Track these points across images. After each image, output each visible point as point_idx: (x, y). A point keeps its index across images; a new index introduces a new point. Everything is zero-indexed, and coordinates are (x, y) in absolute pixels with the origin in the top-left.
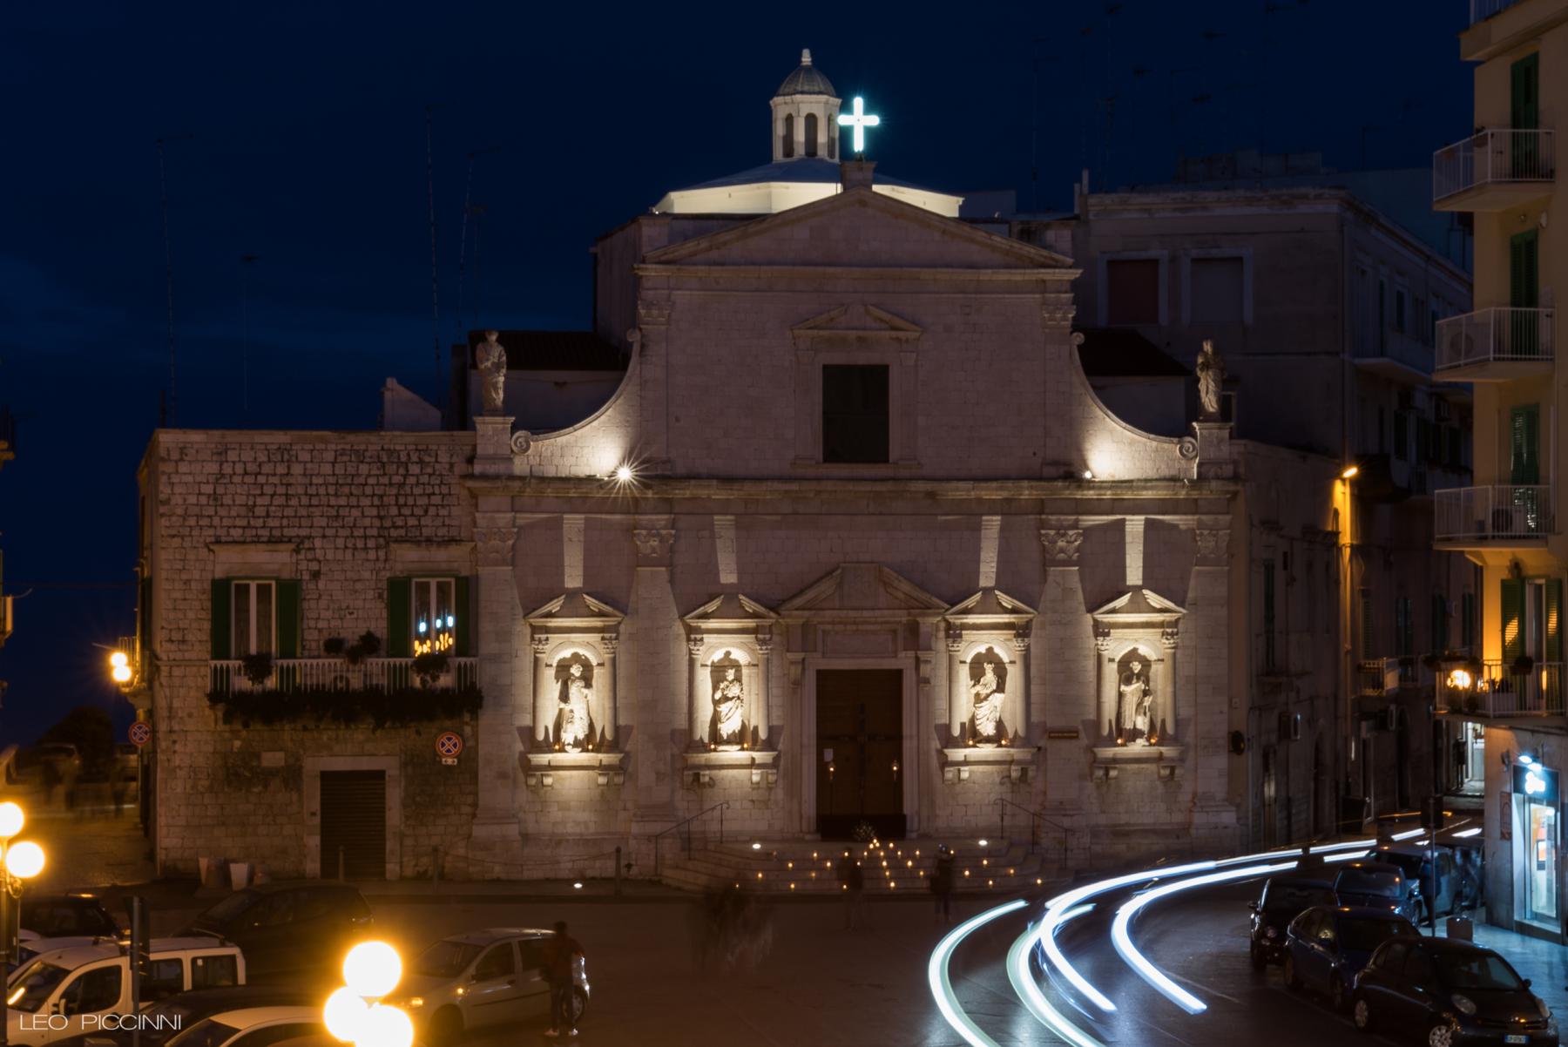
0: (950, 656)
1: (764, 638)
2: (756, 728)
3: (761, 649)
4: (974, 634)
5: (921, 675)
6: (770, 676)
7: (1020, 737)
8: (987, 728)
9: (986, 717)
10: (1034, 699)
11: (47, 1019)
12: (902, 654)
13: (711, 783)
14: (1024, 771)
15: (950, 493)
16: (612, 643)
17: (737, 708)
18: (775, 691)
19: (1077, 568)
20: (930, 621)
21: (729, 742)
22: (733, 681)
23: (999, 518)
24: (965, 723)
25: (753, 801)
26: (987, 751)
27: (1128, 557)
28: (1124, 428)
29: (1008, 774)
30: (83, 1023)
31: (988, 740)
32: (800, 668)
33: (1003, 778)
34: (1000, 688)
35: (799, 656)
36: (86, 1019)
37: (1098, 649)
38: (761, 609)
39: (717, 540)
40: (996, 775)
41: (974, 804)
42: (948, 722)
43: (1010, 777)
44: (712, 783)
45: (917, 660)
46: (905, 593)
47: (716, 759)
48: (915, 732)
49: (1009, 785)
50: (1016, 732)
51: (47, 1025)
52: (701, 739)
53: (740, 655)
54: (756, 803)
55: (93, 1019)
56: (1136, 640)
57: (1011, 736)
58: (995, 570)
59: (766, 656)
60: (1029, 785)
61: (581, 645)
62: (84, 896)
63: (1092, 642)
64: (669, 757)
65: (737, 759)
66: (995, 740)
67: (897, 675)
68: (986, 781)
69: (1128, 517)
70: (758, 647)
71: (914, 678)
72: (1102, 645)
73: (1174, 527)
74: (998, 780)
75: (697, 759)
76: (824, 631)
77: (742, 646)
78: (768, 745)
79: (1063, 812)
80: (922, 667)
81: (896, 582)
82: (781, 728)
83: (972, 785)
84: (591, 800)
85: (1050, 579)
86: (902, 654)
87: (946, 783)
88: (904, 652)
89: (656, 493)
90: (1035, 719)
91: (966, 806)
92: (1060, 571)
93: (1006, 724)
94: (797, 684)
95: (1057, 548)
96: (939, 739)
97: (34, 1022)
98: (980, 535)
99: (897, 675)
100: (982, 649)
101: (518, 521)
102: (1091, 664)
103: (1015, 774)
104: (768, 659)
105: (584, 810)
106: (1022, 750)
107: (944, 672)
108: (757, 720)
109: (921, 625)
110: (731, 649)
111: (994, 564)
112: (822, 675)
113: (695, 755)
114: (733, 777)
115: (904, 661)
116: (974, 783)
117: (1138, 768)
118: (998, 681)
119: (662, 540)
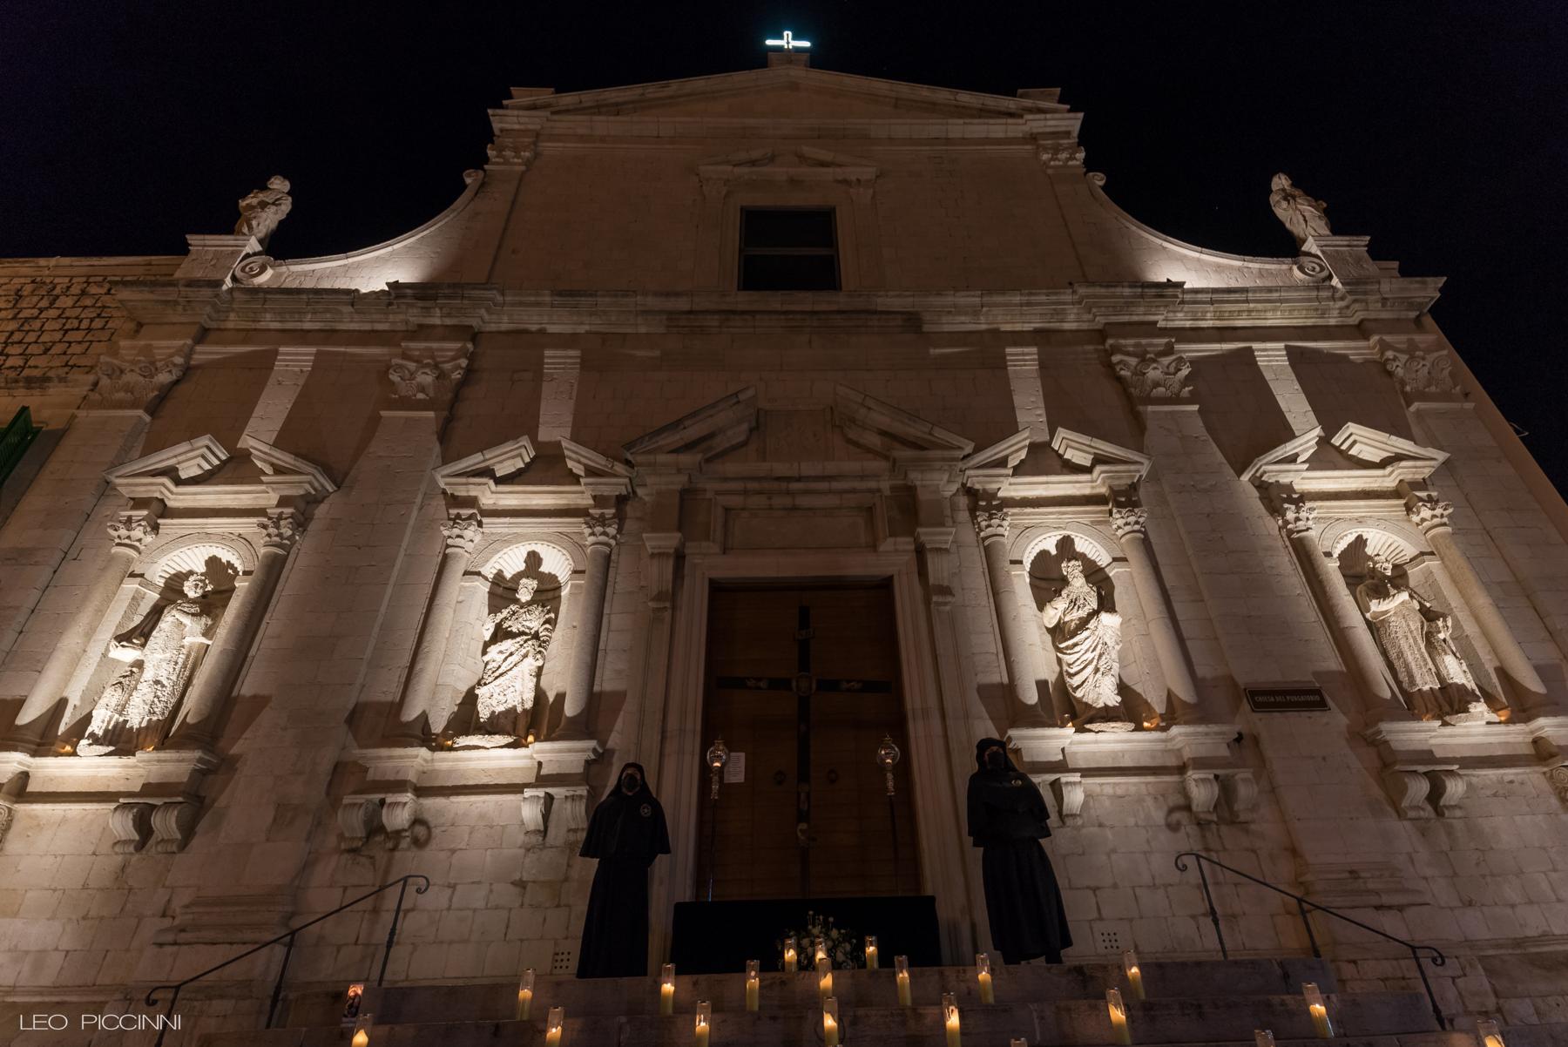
0: (987, 549)
1: (602, 515)
2: (561, 697)
3: (593, 534)
4: (1029, 514)
5: (931, 581)
6: (609, 592)
7: (1184, 703)
8: (1104, 693)
9: (1090, 669)
10: (1187, 630)
11: (47, 1019)
12: (887, 545)
13: (420, 831)
14: (1227, 789)
15: (944, 319)
16: (278, 527)
17: (525, 656)
18: (617, 619)
19: (1196, 407)
20: (942, 484)
21: (494, 726)
22: (529, 603)
23: (1034, 350)
24: (1046, 682)
25: (521, 884)
26: (1112, 740)
27: (1279, 398)
28: (1201, 252)
29: (1181, 801)
30: (83, 1023)
31: (1107, 715)
32: (669, 565)
33: (1171, 811)
34: (1106, 603)
35: (670, 540)
36: (86, 1019)
37: (1290, 532)
38: (599, 461)
39: (545, 385)
40: (1149, 802)
41: (1115, 886)
42: (1006, 680)
43: (1187, 807)
44: (421, 832)
45: (920, 552)
46: (883, 433)
47: (450, 772)
48: (932, 701)
49: (1192, 829)
50: (1170, 695)
51: (46, 1025)
52: (424, 717)
53: (556, 563)
54: (529, 887)
55: (93, 1019)
56: (1360, 521)
57: (1159, 707)
58: (1044, 419)
59: (607, 550)
60: (1244, 826)
61: (223, 539)
62: (890, 784)
63: (1272, 525)
64: (325, 766)
65: (501, 771)
66: (1130, 709)
67: (885, 586)
68: (1131, 821)
69: (1255, 346)
70: (587, 531)
71: (918, 590)
72: (1297, 519)
73: (1342, 359)
74: (1159, 816)
75: (390, 764)
76: (727, 510)
77: (559, 539)
78: (581, 727)
79: (1374, 900)
80: (933, 562)
81: (863, 411)
82: (619, 697)
83: (1095, 830)
84: (85, 887)
85: (1151, 425)
86: (887, 545)
87: (1069, 822)
88: (890, 540)
89: (449, 315)
90: (1201, 671)
91: (1095, 890)
92: (1166, 412)
93: (1138, 688)
94: (670, 597)
95: (1149, 382)
96: (992, 719)
97: (34, 1022)
98: (1007, 374)
99: (885, 586)
100: (1049, 544)
101: (195, 356)
102: (1286, 563)
103: (1201, 792)
104: (608, 558)
105: (53, 918)
106: (1201, 729)
107: (980, 582)
108: (563, 678)
109: (919, 491)
110: (540, 548)
111: (1042, 411)
112: (718, 590)
113: (384, 752)
114: (482, 816)
115: (892, 557)
116: (1101, 825)
117: (1500, 781)
118: (1099, 595)
119: (442, 376)
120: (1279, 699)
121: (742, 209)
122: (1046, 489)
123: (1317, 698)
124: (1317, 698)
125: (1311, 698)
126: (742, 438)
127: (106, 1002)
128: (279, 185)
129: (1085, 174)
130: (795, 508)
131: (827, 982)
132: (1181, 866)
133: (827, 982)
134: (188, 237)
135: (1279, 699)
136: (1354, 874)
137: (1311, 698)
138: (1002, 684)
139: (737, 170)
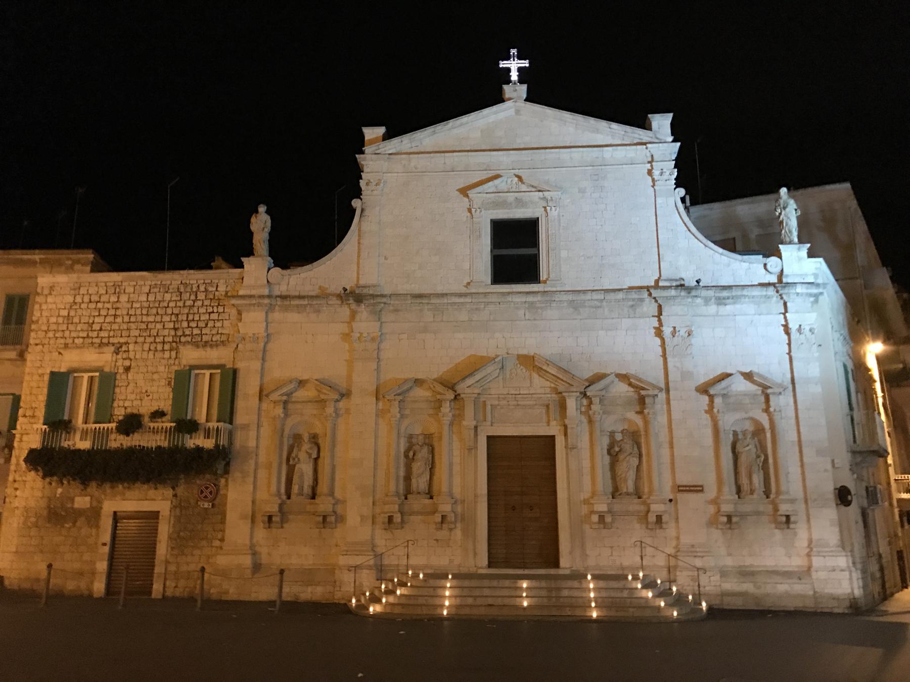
120: (687, 488)
121: (491, 220)
122: (807, 288)
123: (701, 488)
124: (701, 488)
125: (698, 488)
126: (497, 375)
127: (821, 293)
128: (262, 209)
129: (675, 189)
130: (518, 405)
131: (592, 595)
132: (636, 543)
133: (592, 595)
134: (242, 258)
135: (687, 488)
136: (693, 546)
137: (698, 488)
138: (90, 596)
139: (488, 195)
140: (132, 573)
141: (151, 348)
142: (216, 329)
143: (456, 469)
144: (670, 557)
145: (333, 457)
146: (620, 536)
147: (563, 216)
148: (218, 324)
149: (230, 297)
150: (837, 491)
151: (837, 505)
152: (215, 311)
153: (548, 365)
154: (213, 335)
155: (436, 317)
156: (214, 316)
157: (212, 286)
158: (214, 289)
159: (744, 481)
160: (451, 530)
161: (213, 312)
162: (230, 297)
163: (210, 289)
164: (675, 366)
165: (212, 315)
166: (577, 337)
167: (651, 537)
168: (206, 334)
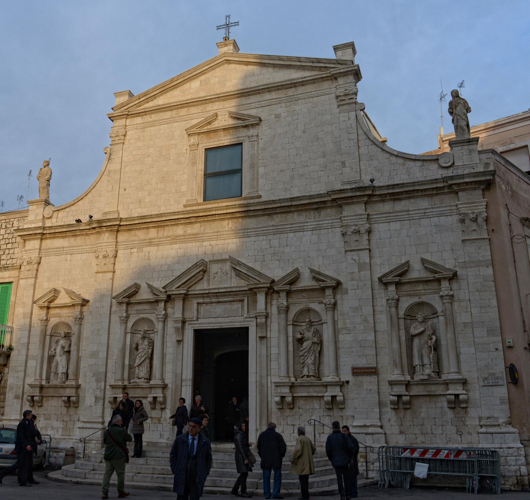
123: (374, 370)
140: (224, 140)
141: (456, 265)
142: (10, 255)
143: (169, 358)
144: (110, 275)
145: (78, 350)
146: (301, 415)
147: (261, 139)
148: (11, 251)
149: (319, 375)
150: (508, 369)
151: (508, 383)
152: (10, 242)
153: (240, 265)
154: (8, 260)
155: (159, 233)
156: (9, 246)
157: (10, 224)
158: (11, 226)
159: (416, 361)
160: (163, 409)
161: (9, 243)
162: (319, 375)
163: (8, 226)
164: (352, 259)
165: (8, 245)
166: (270, 240)
167: (328, 416)
168: (4, 260)
